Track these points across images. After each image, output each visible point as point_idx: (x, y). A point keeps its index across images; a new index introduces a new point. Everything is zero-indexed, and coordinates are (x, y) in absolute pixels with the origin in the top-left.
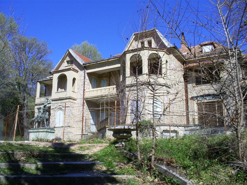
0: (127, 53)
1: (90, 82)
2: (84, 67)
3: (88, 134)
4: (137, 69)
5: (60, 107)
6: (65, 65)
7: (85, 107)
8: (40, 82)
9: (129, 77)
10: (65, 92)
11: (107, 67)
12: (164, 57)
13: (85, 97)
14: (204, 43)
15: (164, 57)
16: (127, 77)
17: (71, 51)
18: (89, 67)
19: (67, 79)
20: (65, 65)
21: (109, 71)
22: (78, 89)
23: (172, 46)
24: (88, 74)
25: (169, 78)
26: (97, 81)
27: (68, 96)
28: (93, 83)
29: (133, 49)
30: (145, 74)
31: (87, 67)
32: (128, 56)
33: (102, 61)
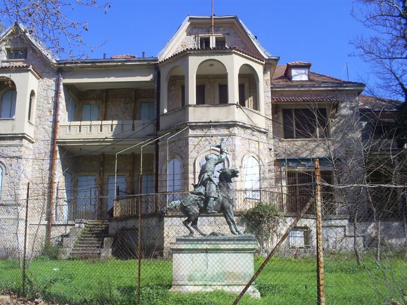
0: (190, 54)
3: (74, 225)
10: (11, 121)
13: (57, 137)
18: (70, 71)
19: (17, 90)
22: (39, 117)
24: (67, 87)
26: (76, 106)
28: (70, 108)
29: (177, 53)
30: (234, 104)
33: (109, 62)
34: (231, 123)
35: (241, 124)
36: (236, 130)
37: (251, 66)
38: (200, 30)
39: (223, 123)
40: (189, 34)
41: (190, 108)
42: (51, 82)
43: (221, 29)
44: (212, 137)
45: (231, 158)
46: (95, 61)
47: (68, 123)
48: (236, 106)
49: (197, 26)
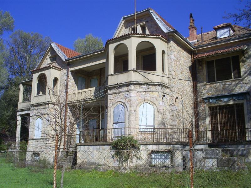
0: (110, 43)
1: (75, 82)
2: (67, 64)
4: (122, 64)
5: (39, 114)
6: (47, 61)
7: (68, 114)
8: (23, 84)
9: (112, 75)
10: (45, 95)
11: (91, 63)
12: (159, 44)
13: (68, 101)
14: (219, 26)
15: (159, 44)
16: (109, 75)
17: (53, 45)
20: (47, 61)
21: (99, 68)
23: (170, 30)
24: (72, 72)
25: (166, 75)
27: (48, 100)
30: (131, 70)
31: (70, 63)
32: (112, 47)
33: (86, 55)
34: (128, 83)
35: (135, 82)
36: (132, 87)
37: (116, 46)
38: (132, 23)
39: (124, 84)
40: (126, 28)
41: (109, 77)
42: (65, 71)
43: (143, 19)
44: (119, 93)
45: (129, 105)
46: (80, 56)
47: (78, 91)
48: (132, 71)
49: (131, 21)
